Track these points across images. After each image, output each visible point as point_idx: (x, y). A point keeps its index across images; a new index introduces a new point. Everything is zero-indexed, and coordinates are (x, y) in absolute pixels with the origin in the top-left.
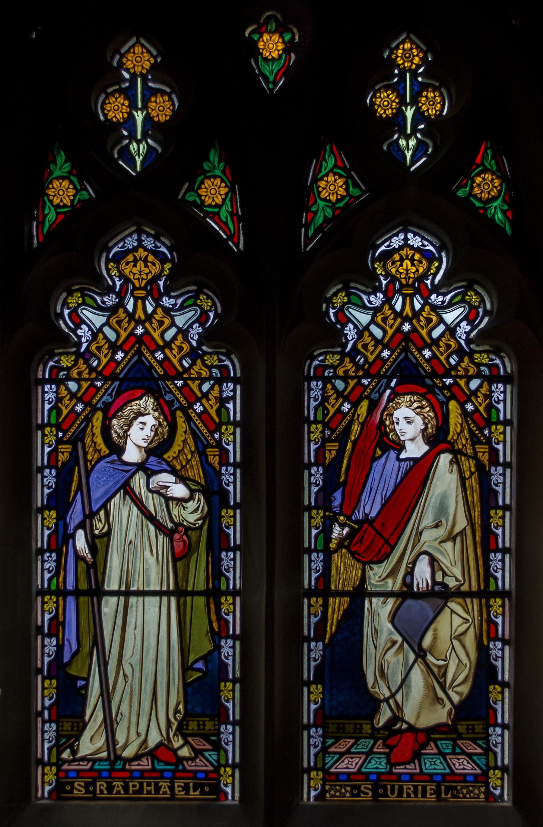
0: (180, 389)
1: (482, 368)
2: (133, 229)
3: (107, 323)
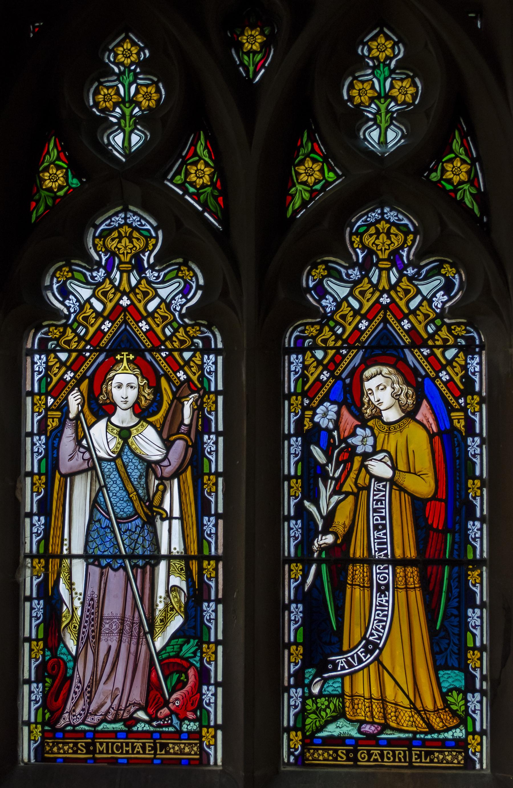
0: (426, 357)
1: (196, 340)
2: (119, 208)
3: (351, 294)
